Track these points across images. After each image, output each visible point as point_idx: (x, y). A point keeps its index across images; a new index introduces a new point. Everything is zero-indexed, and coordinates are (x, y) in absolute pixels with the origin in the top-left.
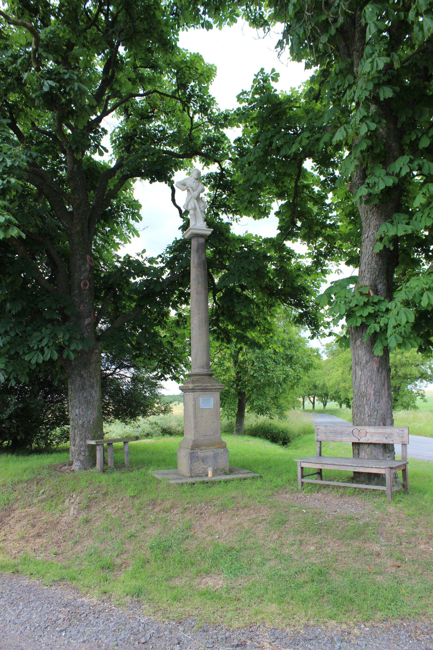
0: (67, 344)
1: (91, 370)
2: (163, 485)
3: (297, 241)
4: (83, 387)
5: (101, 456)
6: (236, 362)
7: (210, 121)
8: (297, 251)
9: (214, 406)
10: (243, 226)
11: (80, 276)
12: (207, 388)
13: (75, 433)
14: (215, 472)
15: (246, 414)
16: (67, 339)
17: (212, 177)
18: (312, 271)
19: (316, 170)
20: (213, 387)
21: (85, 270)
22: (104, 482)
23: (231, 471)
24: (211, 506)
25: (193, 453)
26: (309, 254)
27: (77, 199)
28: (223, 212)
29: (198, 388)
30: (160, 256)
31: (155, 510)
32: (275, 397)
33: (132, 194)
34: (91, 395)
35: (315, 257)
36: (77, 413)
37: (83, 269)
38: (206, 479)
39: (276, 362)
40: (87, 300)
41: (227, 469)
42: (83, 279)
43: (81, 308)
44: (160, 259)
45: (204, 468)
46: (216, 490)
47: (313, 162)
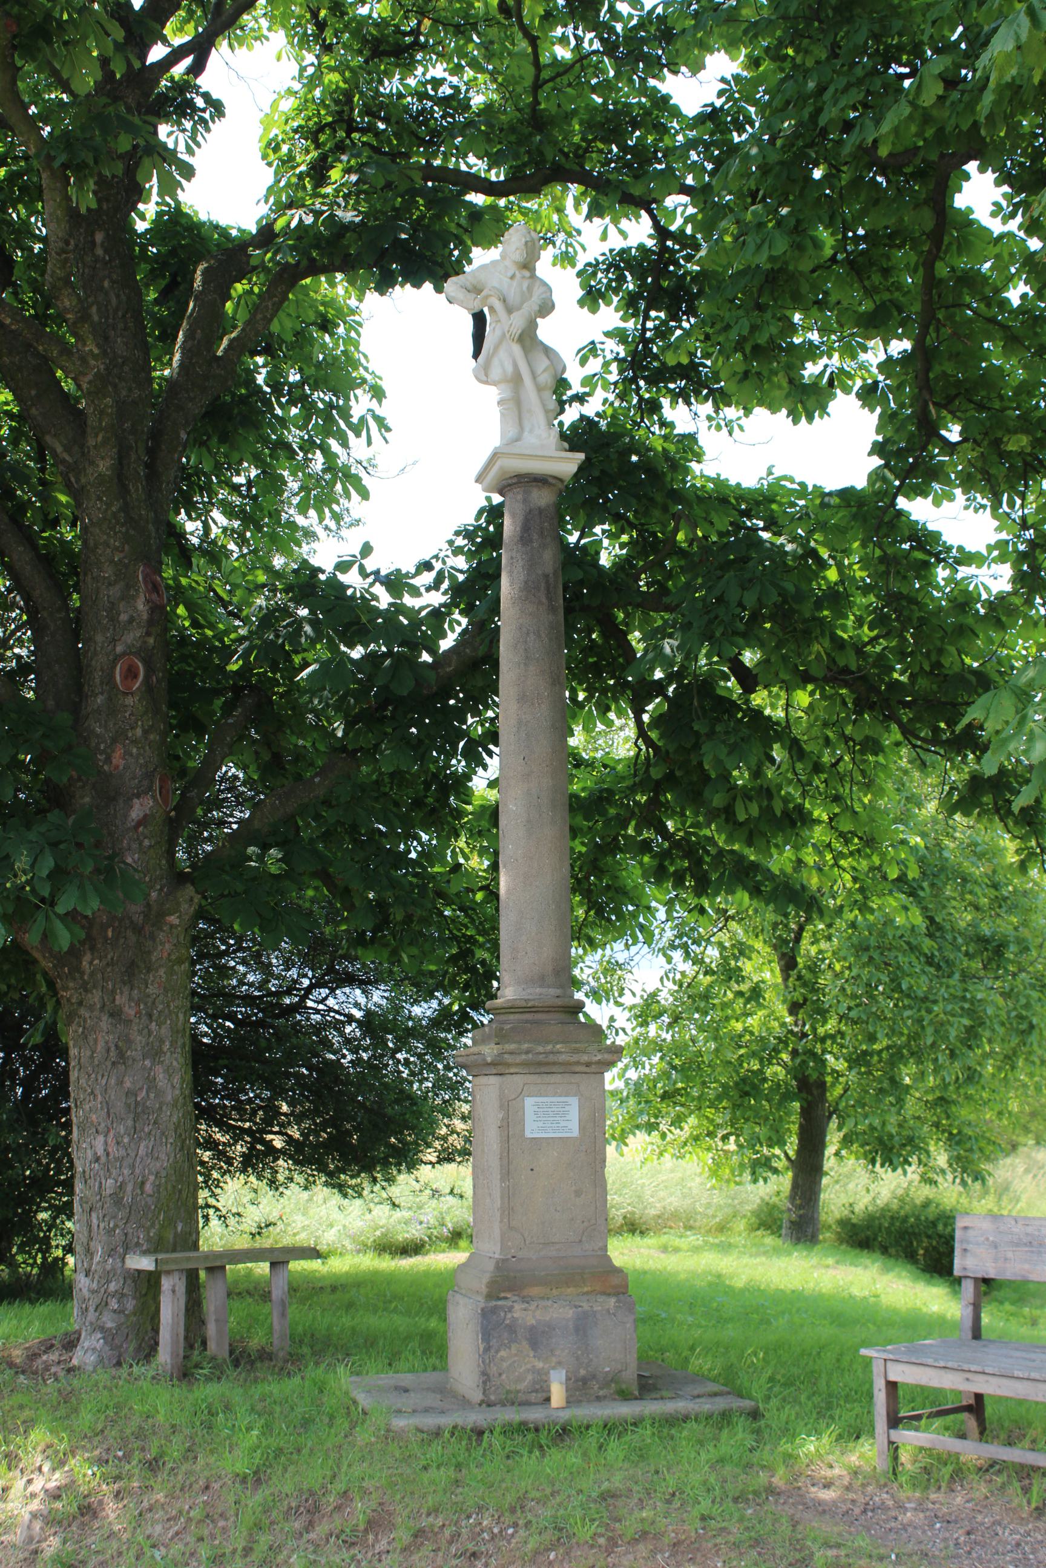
0: (46, 893)
1: (151, 990)
2: (364, 1436)
3: (951, 498)
4: (121, 1055)
5: (175, 1316)
6: (789, 964)
7: (610, 48)
8: (952, 536)
9: (582, 1128)
10: (742, 448)
11: (114, 641)
12: (551, 1058)
13: (90, 1226)
14: (581, 1388)
15: (829, 1162)
16: (45, 873)
17: (627, 262)
18: (1013, 612)
19: (1013, 215)
20: (575, 1058)
21: (131, 620)
22: (161, 1418)
23: (646, 1387)
24: (515, 1525)
25: (494, 1310)
26: (1001, 545)
27: (95, 357)
28: (675, 396)
29: (519, 1059)
30: (427, 566)
31: (312, 1536)
32: (941, 1098)
33: (356, 344)
34: (151, 1082)
35: (1023, 557)
36: (100, 1151)
37: (124, 617)
38: (534, 1415)
39: (939, 968)
40: (139, 732)
41: (630, 1375)
42: (124, 654)
43: (117, 759)
44: (428, 578)
45: (539, 1372)
46: (561, 1460)
47: (998, 183)
